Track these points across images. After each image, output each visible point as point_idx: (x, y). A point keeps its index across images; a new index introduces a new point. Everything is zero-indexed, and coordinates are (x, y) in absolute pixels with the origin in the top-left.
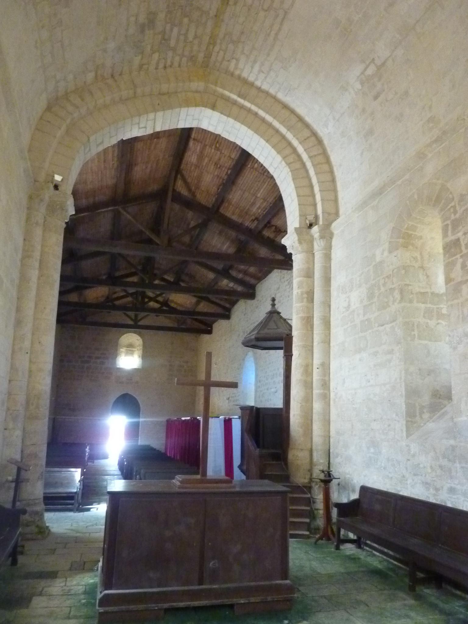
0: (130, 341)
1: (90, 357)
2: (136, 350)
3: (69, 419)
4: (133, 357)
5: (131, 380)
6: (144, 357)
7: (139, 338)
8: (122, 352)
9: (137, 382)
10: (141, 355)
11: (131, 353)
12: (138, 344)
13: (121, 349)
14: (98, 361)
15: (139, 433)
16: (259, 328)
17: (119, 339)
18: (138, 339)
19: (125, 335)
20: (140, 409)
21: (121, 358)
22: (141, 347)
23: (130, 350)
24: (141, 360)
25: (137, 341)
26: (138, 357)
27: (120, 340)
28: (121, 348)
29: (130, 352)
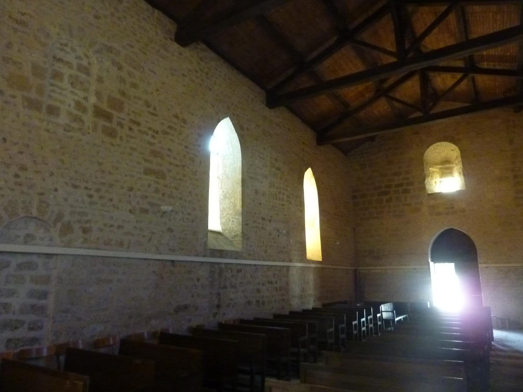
0: (443, 155)
1: (389, 186)
2: (455, 165)
3: (374, 269)
4: (454, 177)
5: (453, 208)
6: (466, 173)
7: (453, 146)
8: (433, 172)
9: (463, 211)
10: (461, 171)
11: (448, 173)
12: (455, 157)
13: (430, 169)
14: (400, 189)
15: (482, 303)
16: (378, 269)
17: (422, 154)
18: (453, 149)
19: (432, 147)
20: (476, 249)
21: (434, 181)
22: (460, 159)
23: (447, 168)
24: (463, 177)
25: (452, 152)
26: (459, 174)
27: (425, 155)
28: (430, 167)
29: (447, 171)
